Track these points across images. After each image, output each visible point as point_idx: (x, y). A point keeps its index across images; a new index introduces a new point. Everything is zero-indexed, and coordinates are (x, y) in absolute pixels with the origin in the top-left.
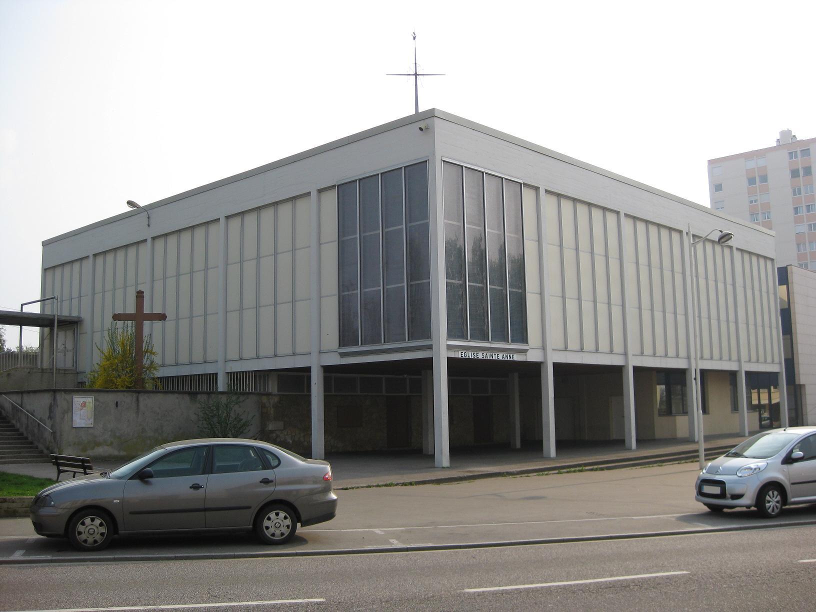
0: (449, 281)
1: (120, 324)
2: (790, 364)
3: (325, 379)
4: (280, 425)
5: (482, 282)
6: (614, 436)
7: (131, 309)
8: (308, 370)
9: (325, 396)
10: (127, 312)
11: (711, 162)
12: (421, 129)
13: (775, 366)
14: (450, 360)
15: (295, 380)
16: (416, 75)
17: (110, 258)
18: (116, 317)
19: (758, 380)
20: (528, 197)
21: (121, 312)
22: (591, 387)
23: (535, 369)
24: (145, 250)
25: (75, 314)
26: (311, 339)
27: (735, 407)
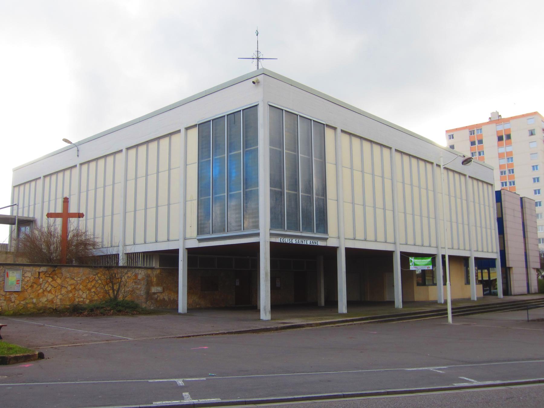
0: (273, 189)
1: (52, 220)
2: (503, 253)
3: (189, 258)
4: (160, 289)
5: (296, 191)
6: (387, 298)
7: (59, 210)
8: (177, 251)
9: (188, 269)
10: (57, 212)
11: (447, 131)
12: (254, 83)
13: (495, 255)
14: (272, 244)
15: (169, 258)
16: (258, 59)
17: (54, 177)
18: (49, 215)
19: (484, 264)
20: (329, 133)
21: (53, 212)
22: (370, 266)
23: (333, 251)
24: (76, 171)
25: (31, 216)
26: (178, 230)
27: (468, 282)
